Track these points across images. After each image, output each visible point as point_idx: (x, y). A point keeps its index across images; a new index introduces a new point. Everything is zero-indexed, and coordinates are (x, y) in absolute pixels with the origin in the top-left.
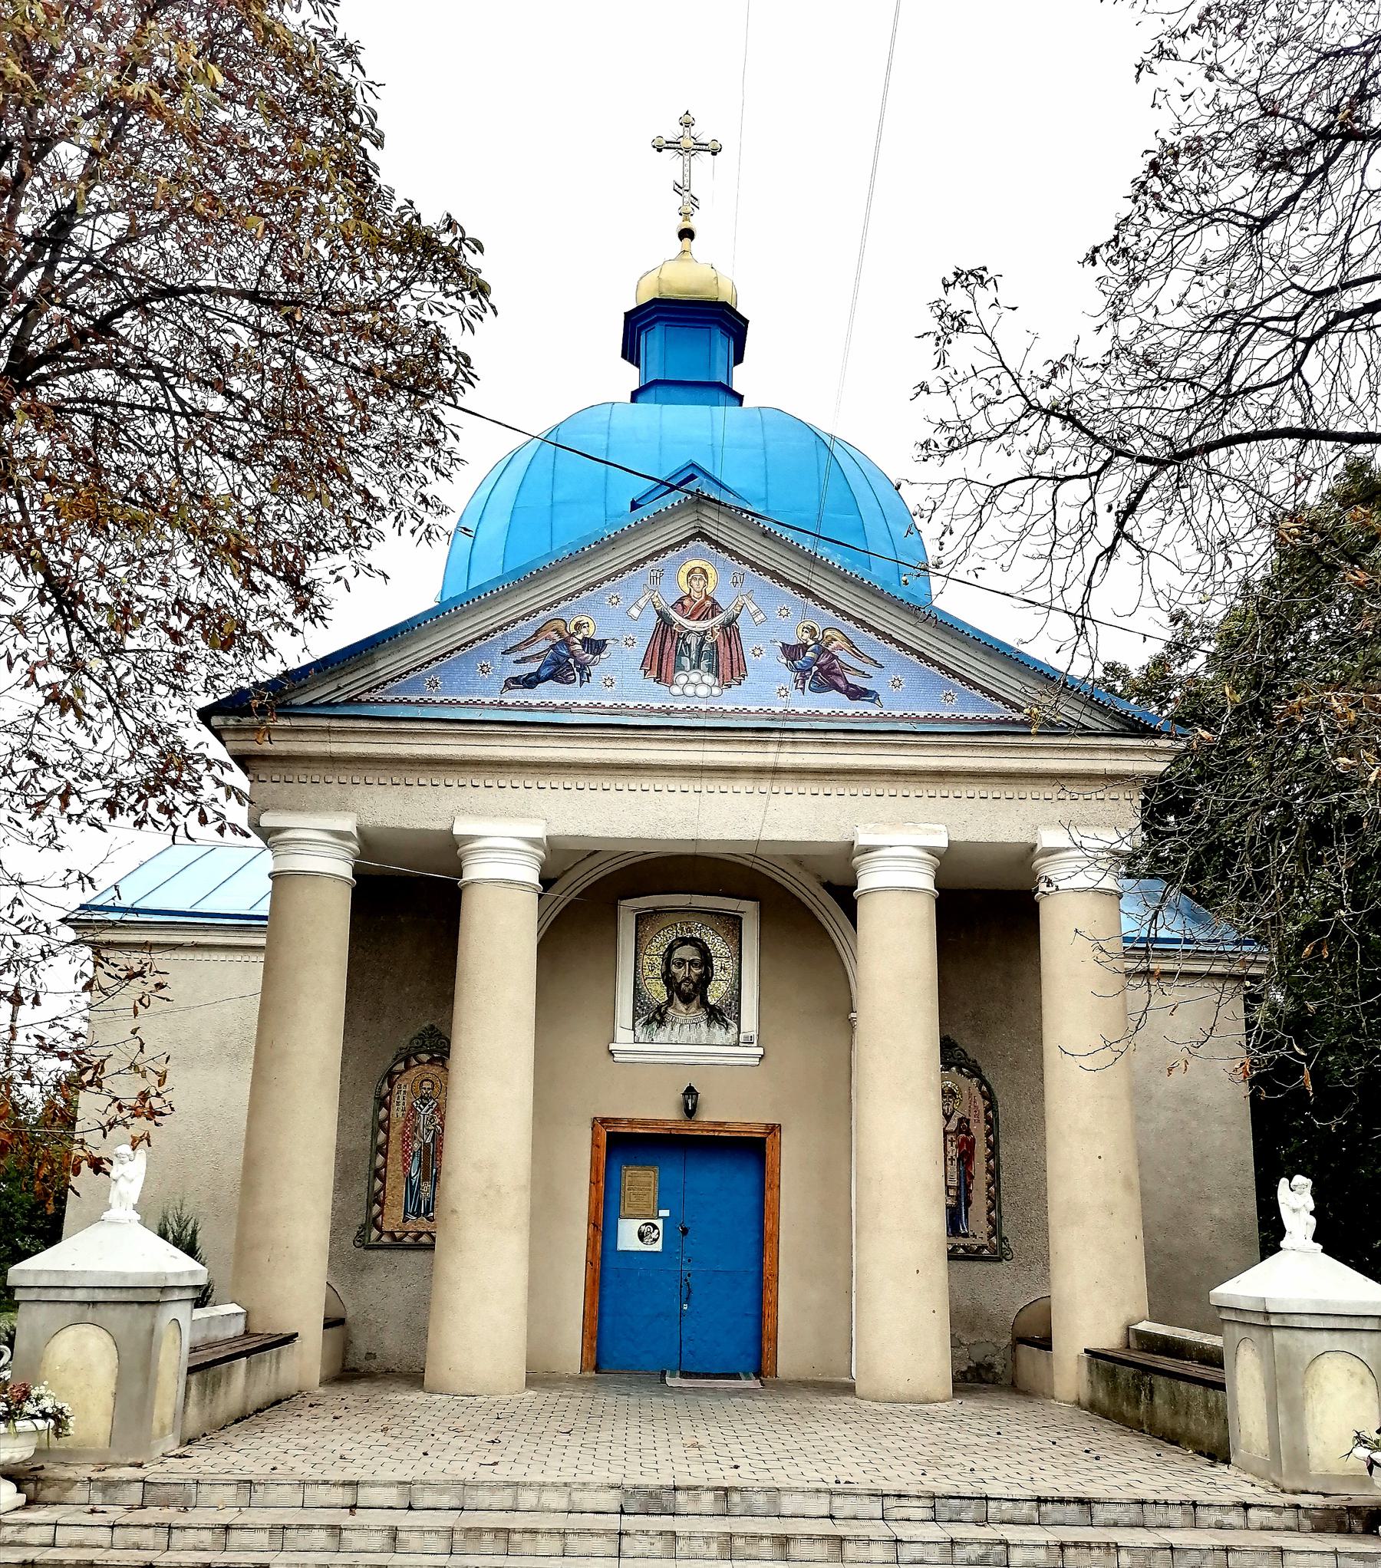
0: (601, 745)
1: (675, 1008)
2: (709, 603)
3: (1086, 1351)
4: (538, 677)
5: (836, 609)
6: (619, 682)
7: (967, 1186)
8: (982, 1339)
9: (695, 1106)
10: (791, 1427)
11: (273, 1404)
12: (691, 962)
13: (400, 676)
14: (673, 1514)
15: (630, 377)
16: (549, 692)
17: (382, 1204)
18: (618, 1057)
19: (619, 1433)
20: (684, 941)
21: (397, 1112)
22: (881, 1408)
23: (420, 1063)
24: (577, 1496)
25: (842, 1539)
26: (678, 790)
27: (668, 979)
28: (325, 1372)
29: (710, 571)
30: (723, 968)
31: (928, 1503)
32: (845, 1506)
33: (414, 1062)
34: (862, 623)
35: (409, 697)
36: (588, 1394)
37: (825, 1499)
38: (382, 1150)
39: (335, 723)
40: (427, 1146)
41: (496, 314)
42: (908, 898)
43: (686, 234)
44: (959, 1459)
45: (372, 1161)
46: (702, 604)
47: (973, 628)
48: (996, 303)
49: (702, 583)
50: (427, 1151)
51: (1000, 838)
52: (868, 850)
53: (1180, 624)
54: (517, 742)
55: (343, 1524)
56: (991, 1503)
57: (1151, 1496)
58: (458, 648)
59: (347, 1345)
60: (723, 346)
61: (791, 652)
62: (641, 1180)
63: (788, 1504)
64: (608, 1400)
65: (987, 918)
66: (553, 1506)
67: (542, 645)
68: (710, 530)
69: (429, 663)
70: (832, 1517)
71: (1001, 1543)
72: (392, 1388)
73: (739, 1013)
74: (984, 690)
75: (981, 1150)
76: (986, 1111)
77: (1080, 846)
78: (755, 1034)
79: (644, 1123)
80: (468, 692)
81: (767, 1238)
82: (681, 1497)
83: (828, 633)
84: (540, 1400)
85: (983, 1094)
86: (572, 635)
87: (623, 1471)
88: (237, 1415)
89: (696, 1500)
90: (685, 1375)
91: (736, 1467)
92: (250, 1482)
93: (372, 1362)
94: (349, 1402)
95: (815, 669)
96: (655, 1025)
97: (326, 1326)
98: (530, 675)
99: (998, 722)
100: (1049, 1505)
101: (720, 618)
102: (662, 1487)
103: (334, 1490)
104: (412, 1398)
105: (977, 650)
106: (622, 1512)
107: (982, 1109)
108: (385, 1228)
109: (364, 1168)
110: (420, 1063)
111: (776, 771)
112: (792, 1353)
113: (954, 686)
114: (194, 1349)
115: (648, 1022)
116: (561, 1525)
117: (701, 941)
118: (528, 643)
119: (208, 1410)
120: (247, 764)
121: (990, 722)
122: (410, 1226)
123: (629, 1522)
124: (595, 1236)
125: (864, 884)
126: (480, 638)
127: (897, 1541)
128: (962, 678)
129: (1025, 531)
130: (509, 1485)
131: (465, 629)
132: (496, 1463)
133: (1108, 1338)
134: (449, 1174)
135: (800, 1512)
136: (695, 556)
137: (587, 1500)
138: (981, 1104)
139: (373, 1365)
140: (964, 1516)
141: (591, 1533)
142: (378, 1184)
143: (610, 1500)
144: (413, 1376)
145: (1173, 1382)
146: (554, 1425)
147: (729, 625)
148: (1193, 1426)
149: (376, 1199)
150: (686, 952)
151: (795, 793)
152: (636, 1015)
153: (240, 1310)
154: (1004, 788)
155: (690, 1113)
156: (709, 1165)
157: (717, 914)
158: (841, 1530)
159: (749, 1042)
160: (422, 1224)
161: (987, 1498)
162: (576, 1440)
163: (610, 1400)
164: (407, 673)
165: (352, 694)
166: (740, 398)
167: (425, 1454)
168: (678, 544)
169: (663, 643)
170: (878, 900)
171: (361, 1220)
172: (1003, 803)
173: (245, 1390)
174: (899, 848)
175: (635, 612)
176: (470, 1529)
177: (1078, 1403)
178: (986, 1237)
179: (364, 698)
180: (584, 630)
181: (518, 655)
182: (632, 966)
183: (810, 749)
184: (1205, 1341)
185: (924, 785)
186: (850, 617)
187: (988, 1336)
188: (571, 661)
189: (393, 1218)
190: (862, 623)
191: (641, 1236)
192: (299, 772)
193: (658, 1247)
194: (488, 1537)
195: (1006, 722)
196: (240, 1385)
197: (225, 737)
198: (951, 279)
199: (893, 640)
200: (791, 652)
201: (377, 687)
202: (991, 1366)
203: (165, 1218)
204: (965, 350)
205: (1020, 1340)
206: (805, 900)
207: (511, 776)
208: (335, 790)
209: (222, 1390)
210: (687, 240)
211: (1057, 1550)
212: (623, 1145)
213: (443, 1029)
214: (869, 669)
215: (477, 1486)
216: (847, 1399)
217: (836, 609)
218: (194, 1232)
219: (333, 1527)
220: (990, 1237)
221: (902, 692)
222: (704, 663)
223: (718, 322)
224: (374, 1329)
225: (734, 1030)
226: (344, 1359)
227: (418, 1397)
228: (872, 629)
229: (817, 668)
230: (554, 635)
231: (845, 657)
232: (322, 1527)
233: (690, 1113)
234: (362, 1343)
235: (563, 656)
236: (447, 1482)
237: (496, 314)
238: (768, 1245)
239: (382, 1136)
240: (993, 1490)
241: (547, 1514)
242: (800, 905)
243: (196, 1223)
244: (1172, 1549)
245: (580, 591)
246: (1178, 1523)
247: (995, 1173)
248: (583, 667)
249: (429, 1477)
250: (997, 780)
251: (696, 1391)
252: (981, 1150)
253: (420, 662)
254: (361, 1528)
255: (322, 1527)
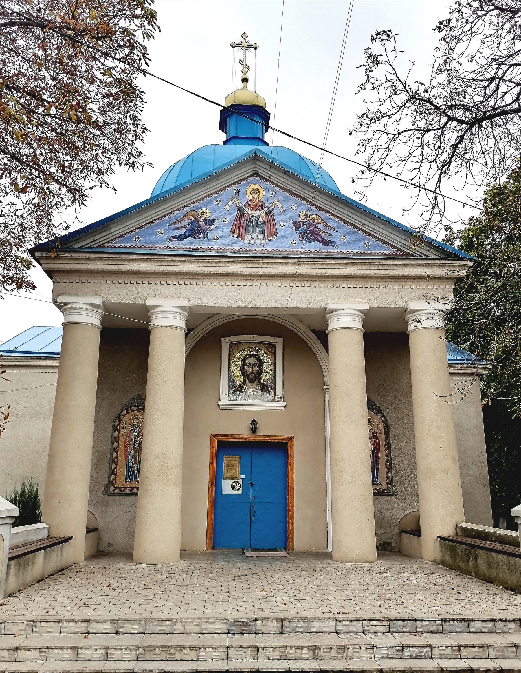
0: (213, 265)
1: (246, 385)
2: (260, 204)
3: (438, 537)
4: (185, 236)
5: (316, 206)
6: (220, 238)
7: (377, 463)
8: (385, 531)
9: (256, 428)
10: (307, 579)
11: (59, 571)
12: (254, 365)
13: (122, 236)
14: (255, 633)
15: (224, 137)
16: (189, 243)
17: (115, 475)
18: (221, 407)
19: (225, 584)
20: (251, 356)
21: (123, 433)
22: (346, 566)
23: (133, 411)
24: (204, 625)
25: (345, 647)
26: (248, 285)
27: (244, 372)
28: (87, 554)
29: (261, 190)
30: (268, 367)
31: (386, 623)
32: (343, 627)
33: (130, 411)
34: (328, 212)
35: (126, 245)
36: (209, 562)
37: (333, 622)
38: (116, 450)
39: (92, 255)
40: (136, 448)
41: (160, 31)
42: (352, 332)
43: (245, 80)
44: (393, 596)
45: (111, 455)
46: (257, 204)
47: (377, 213)
48: (394, 50)
49: (257, 195)
50: (136, 451)
51: (392, 306)
52: (333, 311)
53: (449, 232)
54: (175, 264)
55: (80, 645)
56: (418, 622)
57: (498, 617)
58: (148, 223)
59: (99, 540)
60: (260, 127)
61: (297, 225)
62: (232, 462)
63: (315, 626)
64: (220, 565)
65: (386, 344)
66: (192, 630)
67: (186, 222)
68: (260, 171)
69: (135, 230)
70: (337, 632)
71: (428, 646)
72: (118, 561)
73: (275, 387)
74: (382, 241)
75: (383, 446)
76: (385, 429)
77: (427, 309)
78: (282, 396)
79: (233, 436)
80: (152, 243)
81: (289, 486)
82: (259, 624)
83: (313, 216)
84: (187, 566)
85: (383, 421)
86: (200, 217)
87: (228, 609)
88: (39, 578)
89: (267, 625)
90: (254, 550)
91: (285, 604)
92: (33, 621)
93: (108, 548)
94: (97, 569)
95: (308, 232)
96: (238, 393)
97: (87, 532)
98: (181, 235)
99: (389, 255)
100: (447, 623)
101: (265, 210)
102: (249, 619)
103: (77, 624)
104: (127, 566)
105: (380, 223)
106: (228, 633)
107: (383, 428)
108: (117, 486)
109: (107, 460)
110: (133, 411)
111: (293, 277)
112: (301, 539)
113: (369, 239)
114: (11, 549)
115: (235, 392)
116: (196, 643)
117: (258, 355)
118: (180, 221)
119: (21, 578)
120: (52, 274)
121: (386, 254)
122: (128, 485)
123: (234, 639)
124: (212, 488)
125: (332, 326)
126: (158, 219)
127: (374, 647)
128: (373, 236)
129: (411, 154)
130: (169, 620)
131: (151, 215)
132: (163, 606)
133: (448, 531)
134: (144, 460)
135: (320, 630)
136: (253, 183)
137: (211, 627)
138: (382, 426)
139: (111, 549)
140: (404, 630)
141: (212, 647)
142: (114, 466)
143: (222, 627)
144: (128, 554)
145: (489, 553)
146: (193, 580)
147: (269, 213)
148: (501, 575)
149: (113, 472)
150: (251, 361)
151: (300, 286)
152: (229, 388)
153: (46, 526)
154: (392, 283)
155: (254, 432)
156: (262, 455)
157: (265, 344)
158: (344, 642)
159: (279, 400)
160: (134, 484)
161: (416, 620)
162: (204, 589)
163: (220, 565)
164: (125, 234)
165: (100, 244)
166: (267, 144)
167: (128, 601)
168: (247, 178)
169: (240, 221)
170: (338, 334)
171: (106, 482)
172: (392, 290)
173: (43, 566)
174: (347, 311)
175: (227, 207)
176: (147, 647)
177: (435, 561)
178: (386, 485)
179: (106, 245)
180: (205, 216)
181: (175, 226)
182: (228, 367)
183: (307, 266)
184: (499, 532)
185: (357, 283)
186: (323, 210)
187: (388, 530)
188: (199, 229)
189: (120, 481)
190: (328, 212)
191: (233, 487)
192: (75, 278)
193: (240, 492)
194: (157, 651)
195: (392, 254)
196: (40, 563)
197: (42, 262)
198: (375, 36)
199: (342, 220)
200: (297, 225)
201: (112, 240)
202: (390, 543)
203: (25, 483)
204: (380, 73)
205: (403, 531)
206: (303, 337)
207: (173, 279)
208: (92, 286)
209: (30, 567)
210: (245, 82)
211: (457, 649)
212: (224, 446)
213: (143, 396)
214: (332, 232)
215: (152, 621)
216: (329, 561)
217: (316, 206)
218: (37, 489)
219: (74, 647)
220: (388, 485)
221: (345, 241)
222: (258, 230)
223: (258, 114)
224: (111, 533)
225: (273, 395)
226: (98, 546)
227: (129, 566)
228: (332, 214)
229: (310, 232)
230: (191, 217)
231: (321, 227)
232: (68, 647)
233: (254, 432)
234: (106, 538)
235: (196, 226)
236: (137, 619)
237: (160, 31)
238: (289, 490)
239: (115, 444)
240: (419, 616)
241: (189, 636)
242: (302, 339)
243: (38, 486)
244: (516, 646)
245: (203, 198)
246: (512, 630)
247: (389, 456)
248: (204, 232)
249: (128, 617)
250: (389, 280)
251: (260, 559)
252: (383, 446)
253: (131, 229)
254: (90, 648)
255: (68, 647)
